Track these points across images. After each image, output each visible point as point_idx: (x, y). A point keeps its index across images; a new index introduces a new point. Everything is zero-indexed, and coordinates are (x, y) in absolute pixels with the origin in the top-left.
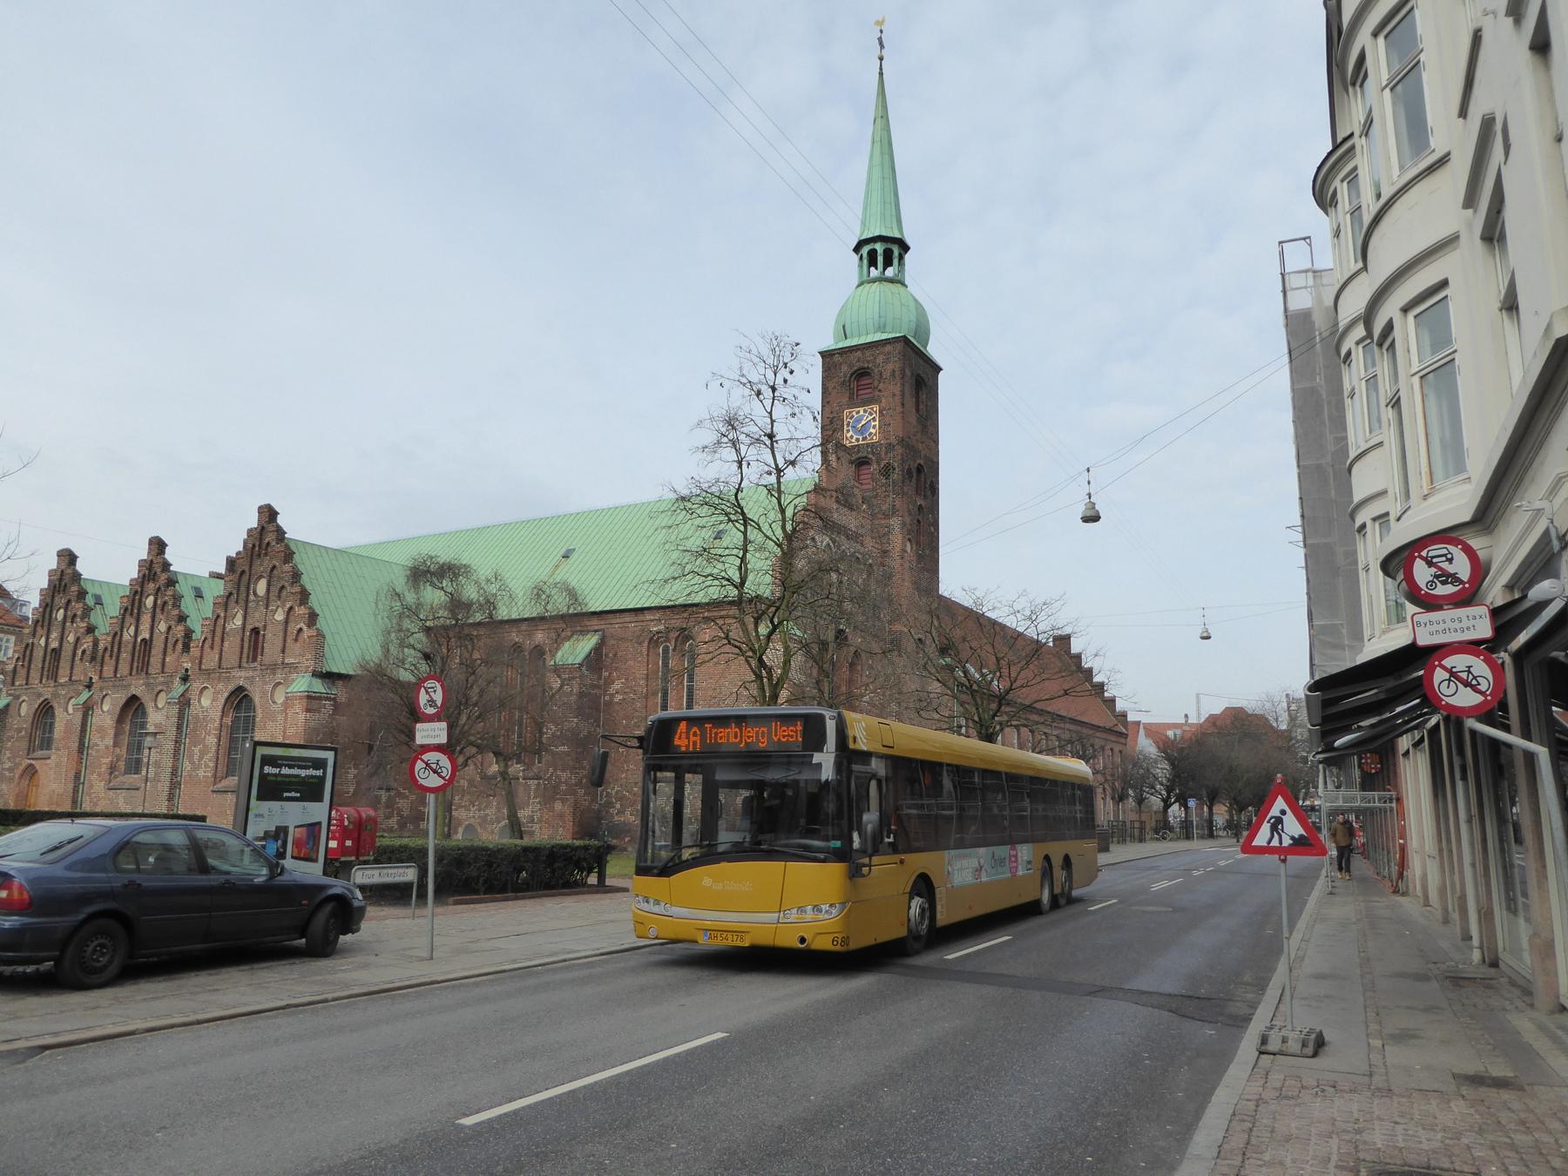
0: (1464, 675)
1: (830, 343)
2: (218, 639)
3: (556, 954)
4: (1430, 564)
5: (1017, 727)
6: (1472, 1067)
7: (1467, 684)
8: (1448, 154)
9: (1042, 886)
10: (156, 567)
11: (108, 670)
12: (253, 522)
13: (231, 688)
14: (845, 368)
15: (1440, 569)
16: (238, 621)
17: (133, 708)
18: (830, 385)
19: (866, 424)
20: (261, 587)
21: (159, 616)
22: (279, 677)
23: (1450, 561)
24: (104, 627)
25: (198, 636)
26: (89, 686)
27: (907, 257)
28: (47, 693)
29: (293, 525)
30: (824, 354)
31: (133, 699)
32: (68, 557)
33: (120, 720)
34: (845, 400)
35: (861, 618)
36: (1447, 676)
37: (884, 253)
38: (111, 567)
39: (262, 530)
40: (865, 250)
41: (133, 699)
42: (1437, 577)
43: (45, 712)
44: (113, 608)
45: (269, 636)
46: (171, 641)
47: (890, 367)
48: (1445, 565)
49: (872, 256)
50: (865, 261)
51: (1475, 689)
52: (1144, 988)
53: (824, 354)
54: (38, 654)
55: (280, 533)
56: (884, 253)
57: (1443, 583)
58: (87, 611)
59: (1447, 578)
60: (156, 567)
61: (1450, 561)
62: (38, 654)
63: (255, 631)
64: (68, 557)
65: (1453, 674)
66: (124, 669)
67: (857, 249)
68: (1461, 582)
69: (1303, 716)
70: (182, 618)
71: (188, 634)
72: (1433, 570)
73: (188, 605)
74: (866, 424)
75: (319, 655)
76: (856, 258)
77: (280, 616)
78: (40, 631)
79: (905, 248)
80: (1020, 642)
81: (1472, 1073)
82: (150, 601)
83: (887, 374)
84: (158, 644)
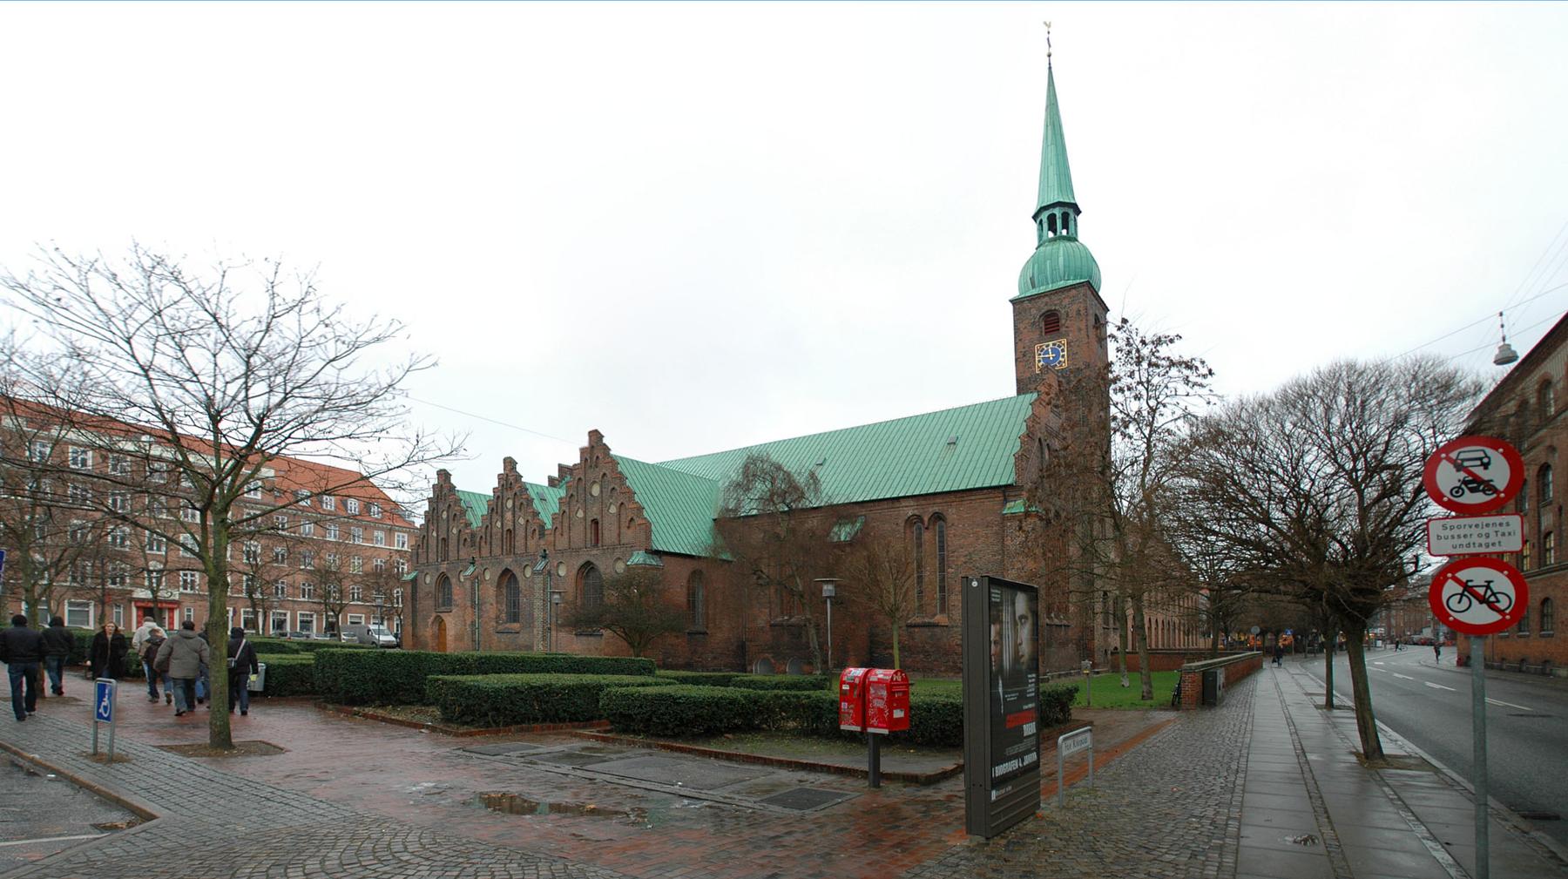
0: (1481, 591)
1: (1015, 294)
2: (566, 529)
3: (624, 777)
4: (1459, 467)
5: (217, 447)
6: (493, 788)
7: (1482, 600)
8: (280, 750)
9: (232, 708)
10: (510, 477)
11: (485, 551)
12: (585, 443)
13: (581, 562)
14: (1034, 311)
15: (1470, 473)
16: (580, 514)
17: (507, 576)
18: (1021, 326)
19: (1054, 353)
20: (596, 490)
21: (518, 513)
22: (617, 554)
23: (1486, 466)
24: (476, 523)
25: (549, 526)
26: (544, 557)
27: (1079, 218)
28: (444, 567)
29: (618, 446)
30: (1014, 302)
31: (506, 571)
32: (510, 463)
33: (499, 586)
34: (1036, 336)
35: (759, 485)
36: (1460, 589)
37: (1058, 217)
38: (477, 480)
39: (592, 447)
40: (1044, 216)
41: (506, 571)
42: (1465, 482)
43: (444, 580)
44: (482, 510)
45: (606, 524)
46: (530, 531)
47: (1075, 307)
48: (1480, 471)
49: (1052, 219)
50: (1045, 226)
51: (1492, 606)
52: (1490, 829)
53: (1014, 302)
54: (433, 543)
55: (606, 449)
56: (1058, 217)
57: (1472, 490)
58: (463, 512)
59: (1476, 484)
60: (510, 477)
61: (1486, 466)
62: (433, 543)
63: (595, 522)
64: (510, 463)
65: (1467, 588)
66: (497, 551)
67: (1035, 217)
68: (1496, 491)
69: (442, 751)
70: (536, 514)
71: (542, 526)
72: (1462, 475)
73: (537, 505)
74: (1054, 353)
75: (648, 538)
76: (1034, 226)
77: (613, 510)
78: (495, 517)
79: (1078, 212)
80: (1512, 760)
81: (252, 759)
82: (510, 504)
83: (1073, 313)
84: (520, 533)
